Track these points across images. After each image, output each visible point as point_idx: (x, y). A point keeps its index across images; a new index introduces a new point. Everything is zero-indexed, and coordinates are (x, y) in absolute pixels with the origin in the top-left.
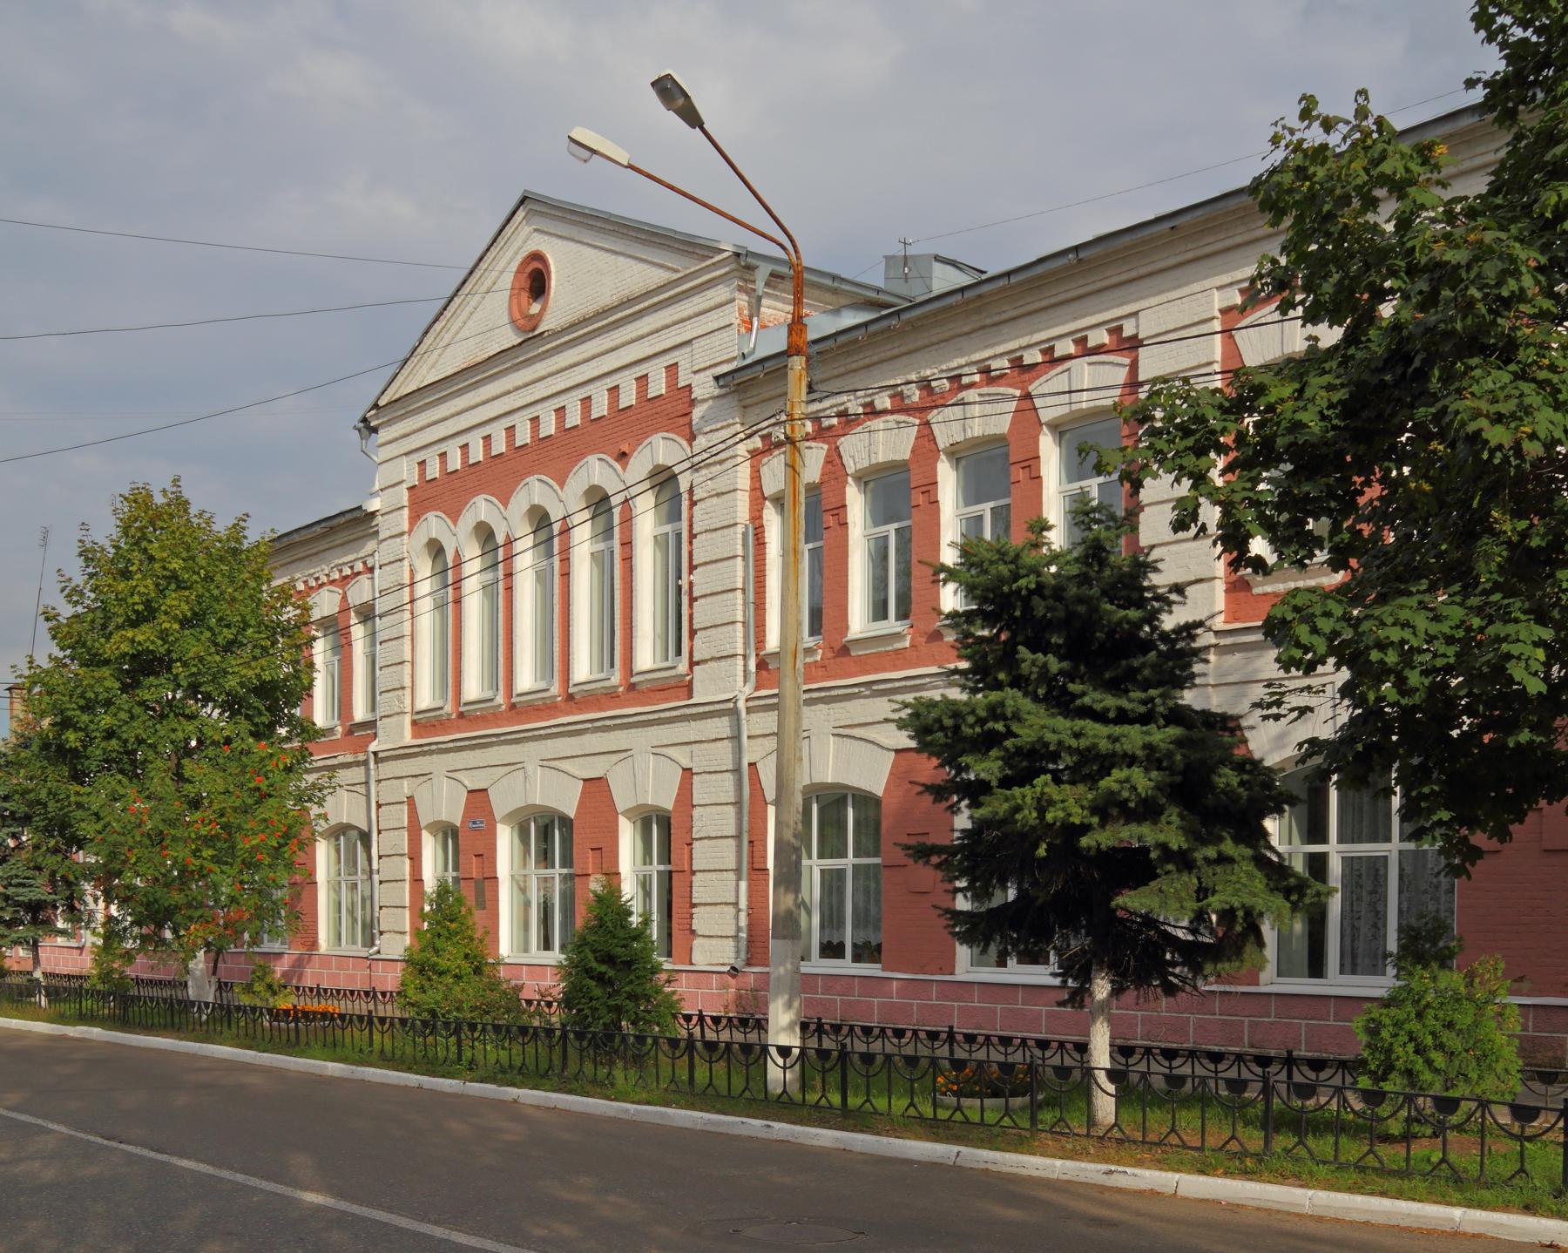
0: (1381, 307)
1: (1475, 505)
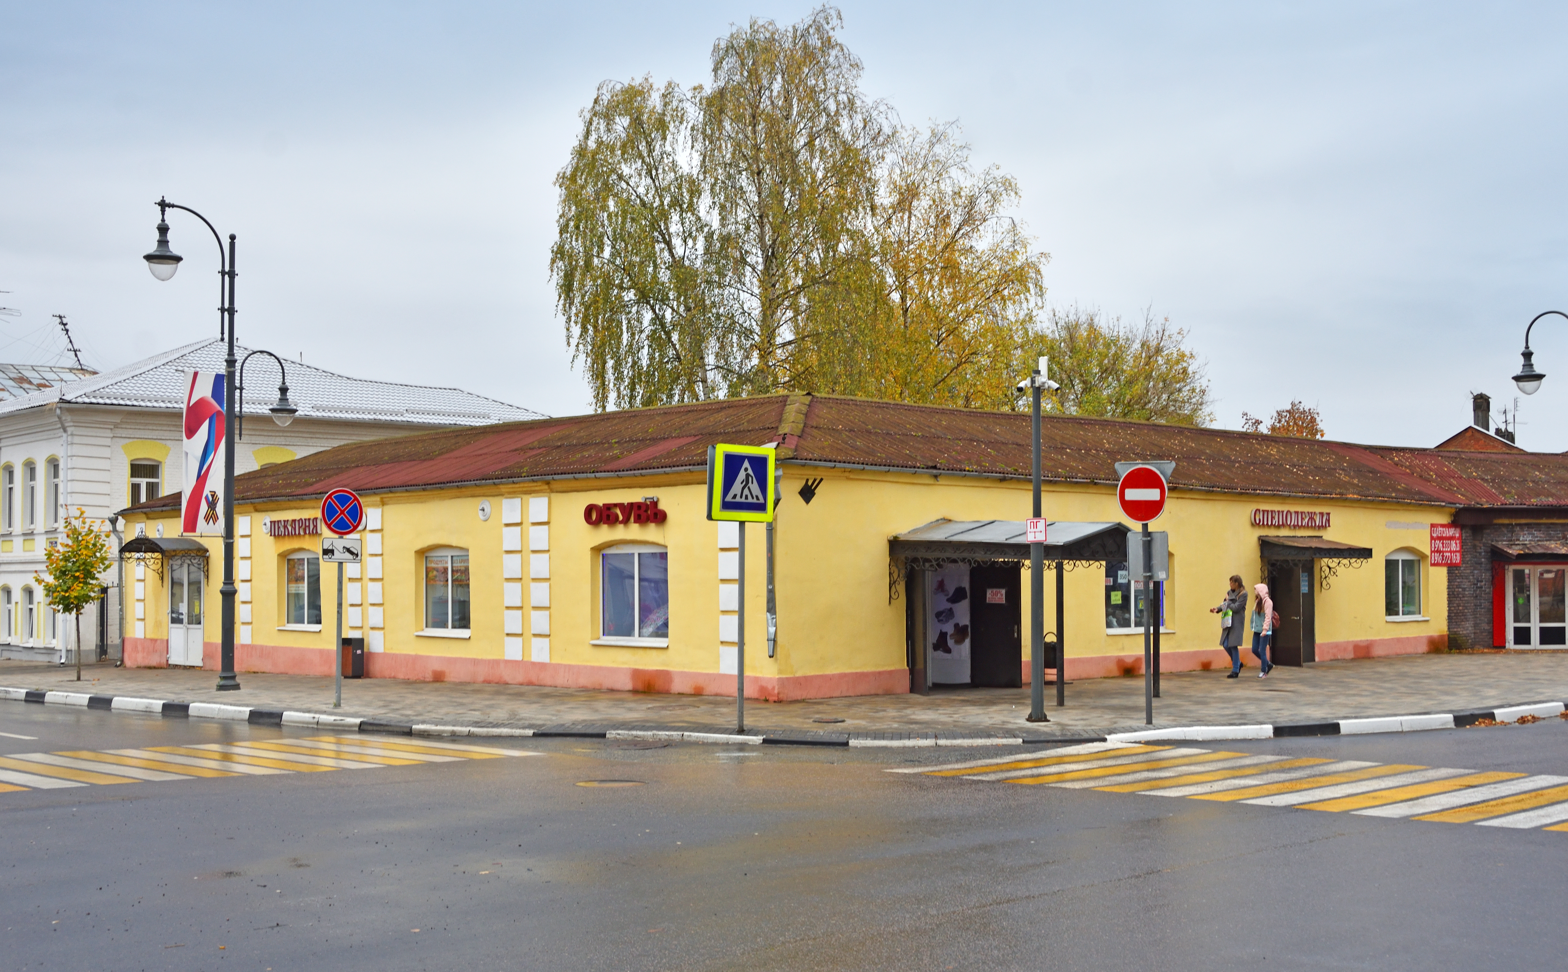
1: (417, 930)
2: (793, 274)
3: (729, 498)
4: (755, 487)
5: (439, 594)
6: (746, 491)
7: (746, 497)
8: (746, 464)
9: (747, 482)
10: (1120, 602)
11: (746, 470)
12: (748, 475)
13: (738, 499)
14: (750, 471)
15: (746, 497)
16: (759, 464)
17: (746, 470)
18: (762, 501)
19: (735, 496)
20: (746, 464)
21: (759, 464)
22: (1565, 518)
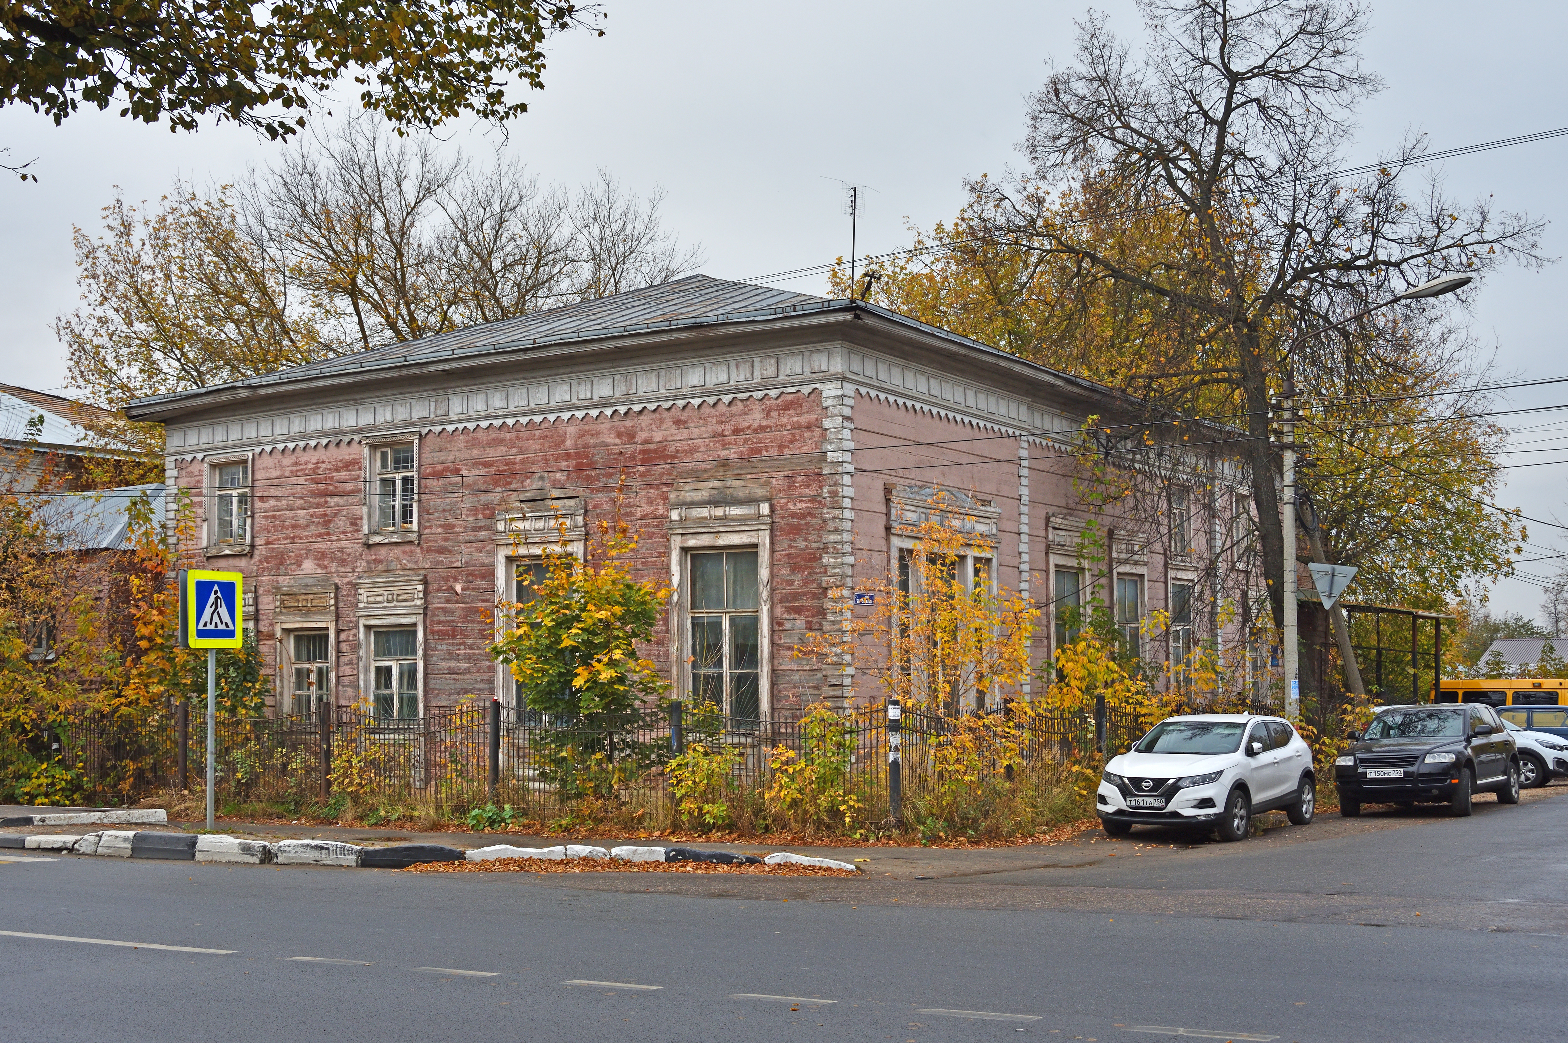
0: (222, 85)
2: (373, 821)
3: (201, 627)
4: (223, 610)
5: (746, 611)
6: (216, 618)
7: (216, 626)
8: (216, 588)
9: (216, 607)
10: (899, 735)
11: (216, 592)
12: (217, 598)
13: (210, 627)
14: (219, 594)
15: (216, 626)
16: (228, 589)
17: (216, 592)
18: (231, 627)
19: (205, 625)
20: (216, 588)
21: (228, 589)
22: (2, 936)
